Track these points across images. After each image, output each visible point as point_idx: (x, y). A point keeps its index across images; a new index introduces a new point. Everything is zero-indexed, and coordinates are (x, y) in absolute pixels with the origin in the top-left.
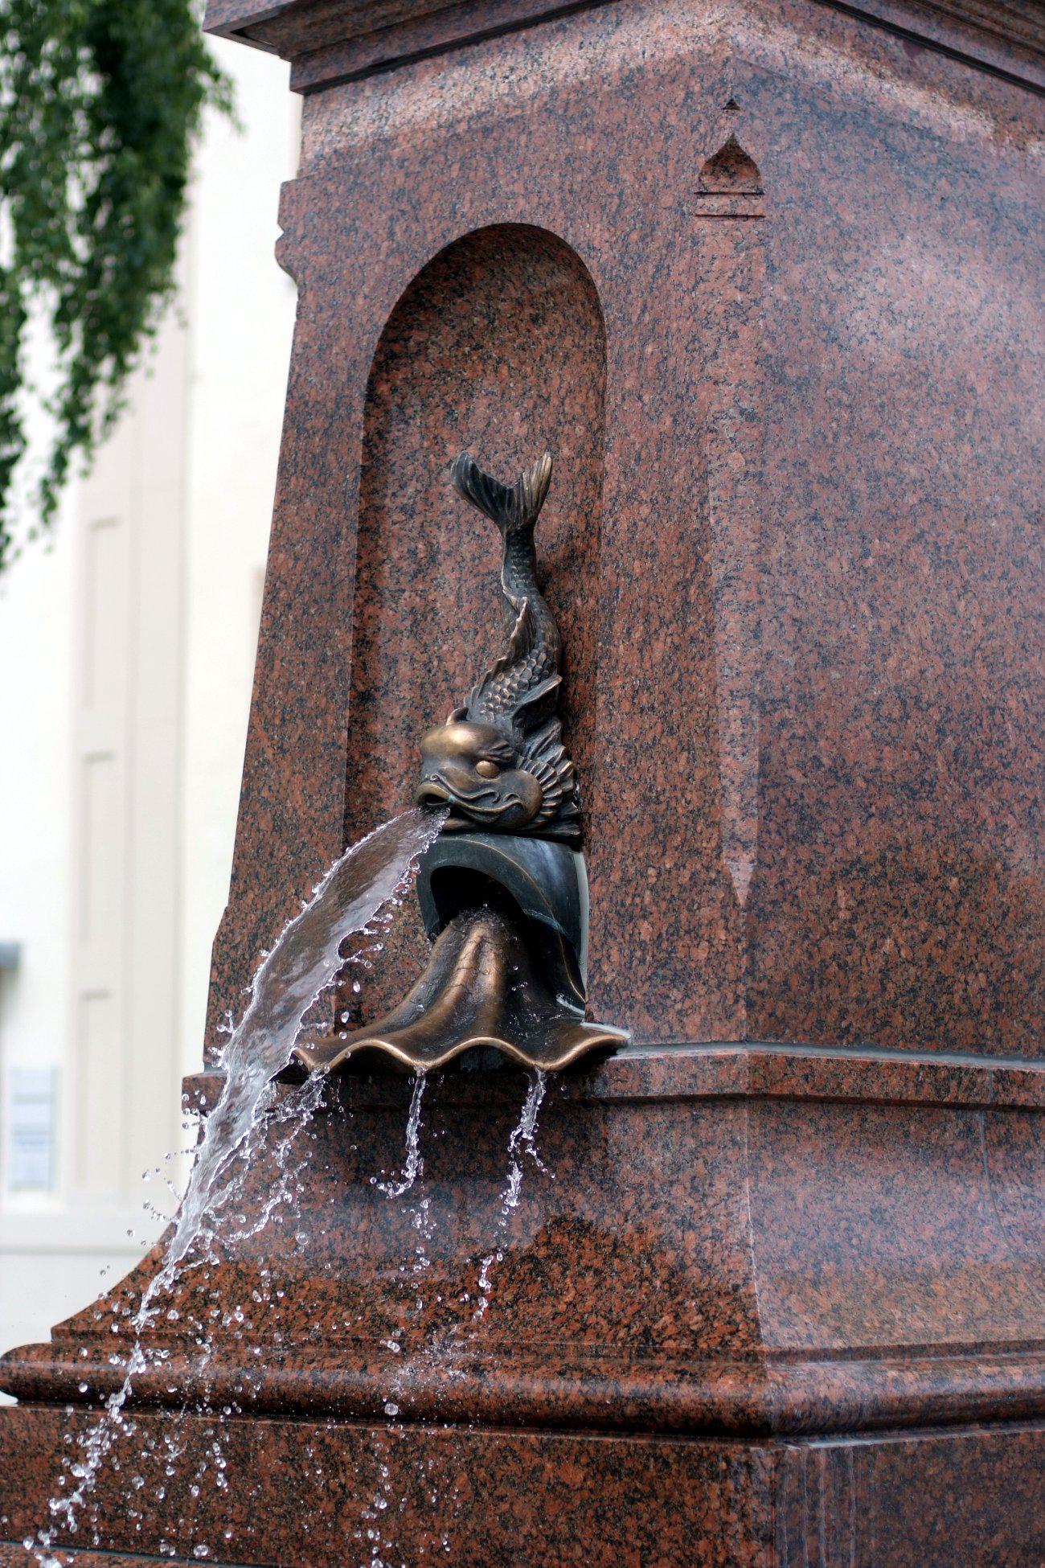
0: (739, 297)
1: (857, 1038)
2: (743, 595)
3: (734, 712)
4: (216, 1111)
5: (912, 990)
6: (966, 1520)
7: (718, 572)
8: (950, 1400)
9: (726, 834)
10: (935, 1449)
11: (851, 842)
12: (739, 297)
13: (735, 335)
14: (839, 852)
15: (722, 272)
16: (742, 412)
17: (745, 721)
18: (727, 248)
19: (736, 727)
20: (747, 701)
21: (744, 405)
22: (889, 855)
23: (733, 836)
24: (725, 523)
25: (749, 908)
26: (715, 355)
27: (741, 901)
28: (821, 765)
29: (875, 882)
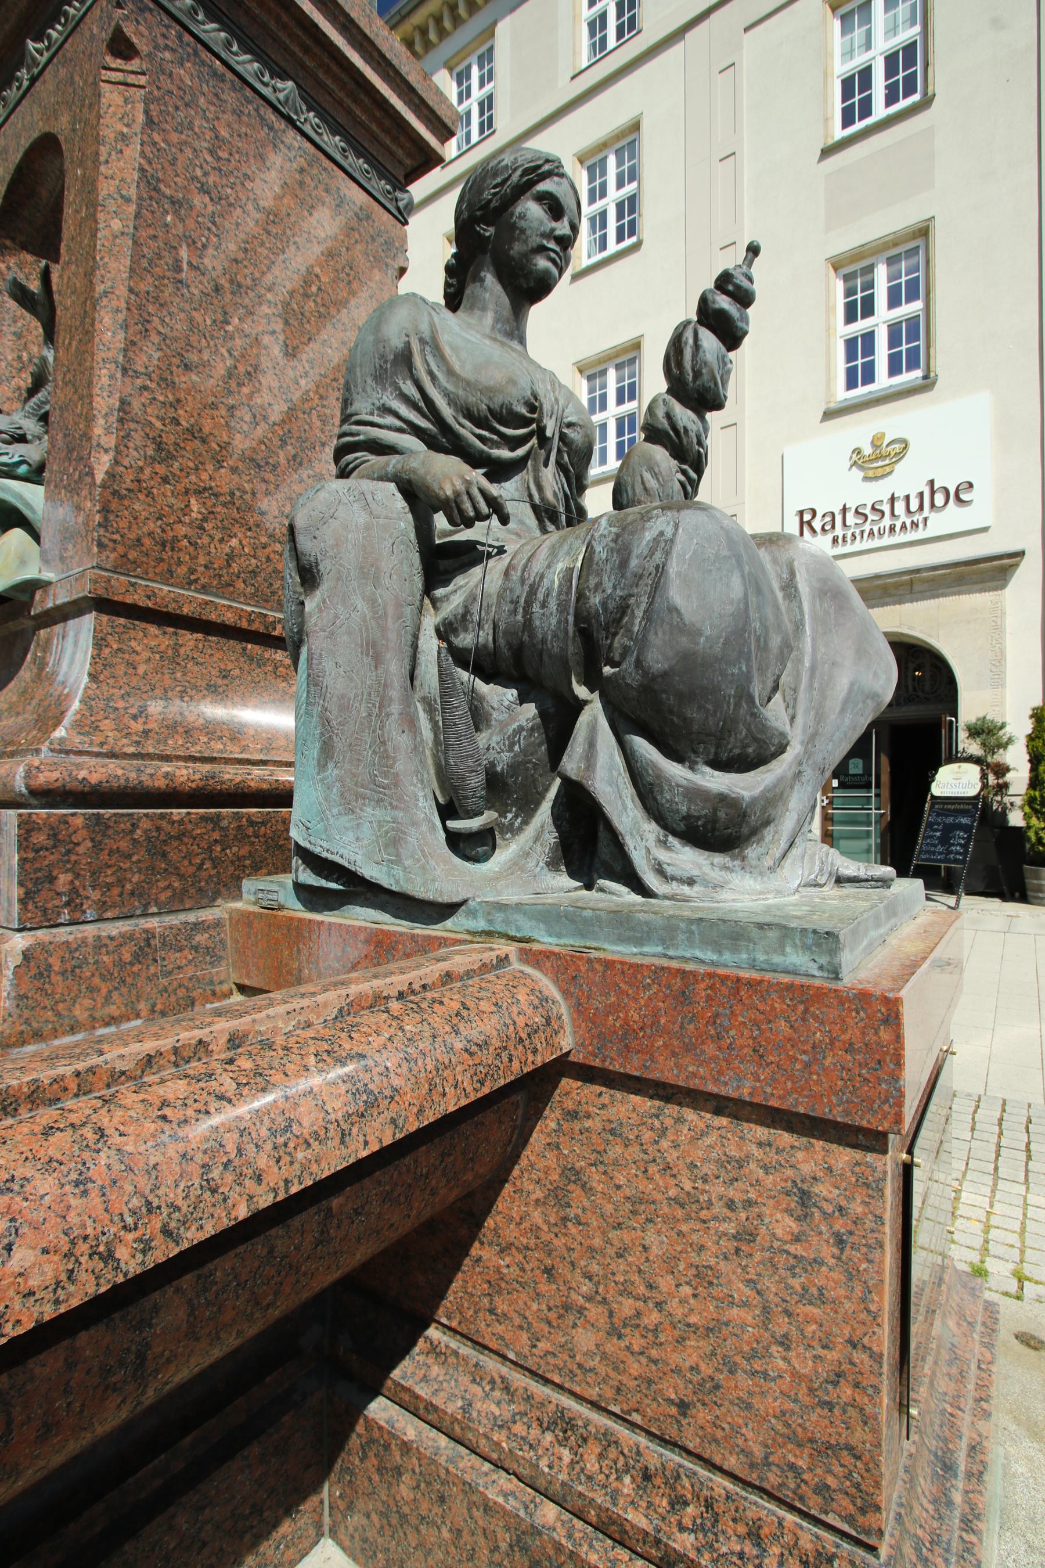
0: (125, 130)
1: (204, 587)
2: (115, 303)
3: (104, 371)
4: (83, 686)
5: (253, 572)
6: (233, 862)
7: (100, 288)
8: (740, 914)
9: (95, 443)
10: (204, 818)
11: (205, 476)
12: (125, 130)
13: (121, 152)
14: (193, 478)
15: (115, 114)
16: (122, 197)
17: (112, 377)
18: (120, 101)
19: (105, 381)
20: (114, 366)
21: (124, 192)
22: (238, 494)
23: (99, 445)
24: (106, 260)
25: (104, 486)
26: (107, 162)
27: (98, 481)
28: (179, 424)
29: (224, 505)
